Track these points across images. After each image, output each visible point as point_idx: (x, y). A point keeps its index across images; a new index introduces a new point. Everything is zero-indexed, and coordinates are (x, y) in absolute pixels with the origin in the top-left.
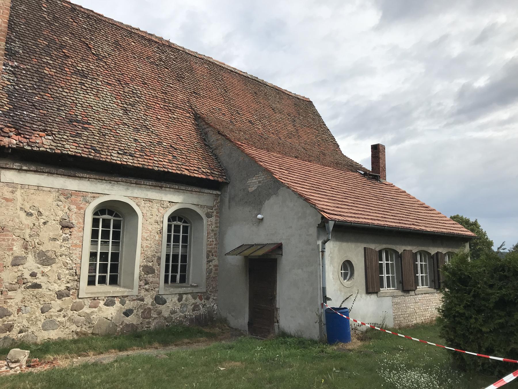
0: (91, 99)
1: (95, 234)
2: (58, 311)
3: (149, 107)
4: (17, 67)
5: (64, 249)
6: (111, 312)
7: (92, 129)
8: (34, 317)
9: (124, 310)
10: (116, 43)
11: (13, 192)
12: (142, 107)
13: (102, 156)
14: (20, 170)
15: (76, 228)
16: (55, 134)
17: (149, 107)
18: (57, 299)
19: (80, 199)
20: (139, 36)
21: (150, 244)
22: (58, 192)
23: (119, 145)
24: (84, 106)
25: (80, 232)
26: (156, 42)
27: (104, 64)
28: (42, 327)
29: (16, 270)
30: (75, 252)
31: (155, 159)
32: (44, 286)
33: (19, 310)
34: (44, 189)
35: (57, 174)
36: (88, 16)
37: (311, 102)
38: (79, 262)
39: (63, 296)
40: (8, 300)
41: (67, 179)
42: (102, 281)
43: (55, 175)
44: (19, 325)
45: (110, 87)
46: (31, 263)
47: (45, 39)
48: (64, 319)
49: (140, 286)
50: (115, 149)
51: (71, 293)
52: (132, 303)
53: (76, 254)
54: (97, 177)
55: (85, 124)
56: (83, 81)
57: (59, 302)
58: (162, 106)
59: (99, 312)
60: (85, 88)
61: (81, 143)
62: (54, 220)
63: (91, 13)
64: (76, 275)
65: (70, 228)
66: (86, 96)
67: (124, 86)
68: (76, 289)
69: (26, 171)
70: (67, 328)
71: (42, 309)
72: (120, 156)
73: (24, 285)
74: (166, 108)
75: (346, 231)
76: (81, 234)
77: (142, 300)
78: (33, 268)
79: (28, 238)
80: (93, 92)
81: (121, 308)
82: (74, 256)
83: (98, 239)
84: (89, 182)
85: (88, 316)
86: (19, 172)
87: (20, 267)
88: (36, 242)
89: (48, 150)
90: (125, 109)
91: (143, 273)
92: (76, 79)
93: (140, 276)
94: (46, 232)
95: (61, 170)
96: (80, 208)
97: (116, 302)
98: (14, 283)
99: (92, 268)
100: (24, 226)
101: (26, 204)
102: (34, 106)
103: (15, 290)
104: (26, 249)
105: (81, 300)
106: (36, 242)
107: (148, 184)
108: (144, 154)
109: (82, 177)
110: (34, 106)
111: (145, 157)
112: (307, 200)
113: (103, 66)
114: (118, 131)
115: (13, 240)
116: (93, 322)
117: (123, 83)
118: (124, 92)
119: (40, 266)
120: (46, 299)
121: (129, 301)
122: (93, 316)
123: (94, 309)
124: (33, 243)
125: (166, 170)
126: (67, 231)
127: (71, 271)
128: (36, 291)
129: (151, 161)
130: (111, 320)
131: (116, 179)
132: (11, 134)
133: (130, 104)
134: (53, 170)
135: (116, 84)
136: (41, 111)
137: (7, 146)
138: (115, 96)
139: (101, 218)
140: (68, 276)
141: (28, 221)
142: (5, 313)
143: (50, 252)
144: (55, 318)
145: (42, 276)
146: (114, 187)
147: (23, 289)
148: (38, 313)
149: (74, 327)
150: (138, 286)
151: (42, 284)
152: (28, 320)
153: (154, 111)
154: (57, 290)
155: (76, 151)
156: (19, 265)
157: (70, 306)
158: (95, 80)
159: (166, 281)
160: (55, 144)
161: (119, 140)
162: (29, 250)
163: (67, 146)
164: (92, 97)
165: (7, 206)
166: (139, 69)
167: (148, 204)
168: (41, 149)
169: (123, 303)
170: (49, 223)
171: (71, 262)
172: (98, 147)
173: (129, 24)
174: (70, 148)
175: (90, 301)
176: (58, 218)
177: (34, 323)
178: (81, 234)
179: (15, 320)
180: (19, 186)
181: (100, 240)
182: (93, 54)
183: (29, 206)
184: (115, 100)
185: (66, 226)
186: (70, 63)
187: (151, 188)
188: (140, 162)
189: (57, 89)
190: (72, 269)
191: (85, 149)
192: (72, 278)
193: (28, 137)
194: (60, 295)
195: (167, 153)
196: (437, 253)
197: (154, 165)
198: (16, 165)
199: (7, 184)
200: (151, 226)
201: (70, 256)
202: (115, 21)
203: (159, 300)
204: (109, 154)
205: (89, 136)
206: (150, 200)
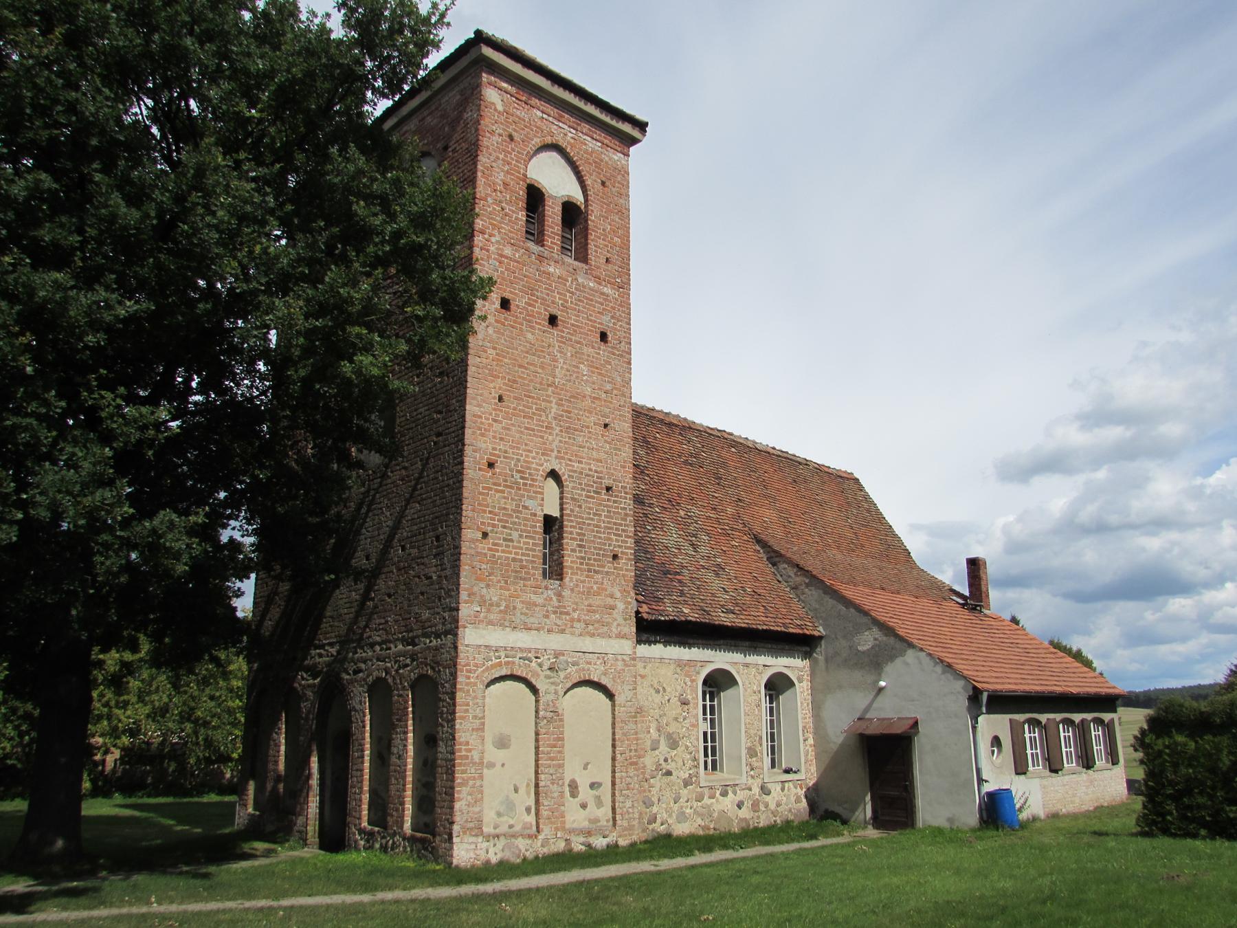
37: (857, 480)
75: (1001, 702)
77: (750, 789)
85: (709, 806)
112: (949, 666)
141: (658, 699)
149: (699, 821)
159: (706, 768)
194: (686, 783)
196: (1083, 721)
203: (765, 790)
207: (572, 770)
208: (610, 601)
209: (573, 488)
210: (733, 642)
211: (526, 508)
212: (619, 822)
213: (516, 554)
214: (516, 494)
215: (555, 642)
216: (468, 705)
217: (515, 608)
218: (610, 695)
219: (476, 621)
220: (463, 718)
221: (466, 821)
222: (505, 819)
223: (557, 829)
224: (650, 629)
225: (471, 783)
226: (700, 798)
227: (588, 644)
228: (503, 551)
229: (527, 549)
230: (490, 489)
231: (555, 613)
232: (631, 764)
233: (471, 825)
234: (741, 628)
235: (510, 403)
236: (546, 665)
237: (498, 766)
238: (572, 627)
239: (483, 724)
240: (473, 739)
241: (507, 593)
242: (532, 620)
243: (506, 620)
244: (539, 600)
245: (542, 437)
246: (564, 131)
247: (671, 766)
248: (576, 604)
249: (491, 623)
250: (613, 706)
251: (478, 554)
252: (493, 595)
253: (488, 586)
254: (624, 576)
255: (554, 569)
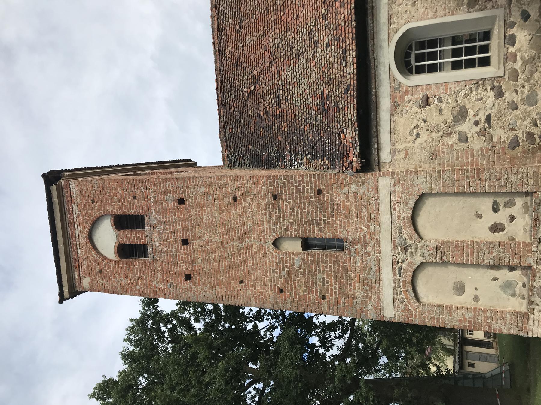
0: (297, 90)
1: (433, 69)
2: (517, 94)
3: (288, 30)
4: (290, 152)
5: (450, 100)
6: (523, 37)
7: (327, 91)
8: (521, 115)
9: (522, 21)
10: (236, 65)
11: (399, 152)
12: (291, 37)
13: (352, 83)
14: (378, 149)
15: (428, 92)
16: (340, 126)
17: (288, 30)
18: (504, 97)
19: (398, 93)
20: (220, 42)
21: (441, 6)
22: (393, 115)
23: (336, 64)
24: (306, 97)
25: (431, 87)
26: (218, 23)
27: (261, 78)
28: (533, 106)
29: (472, 139)
30: (452, 89)
31: (343, 25)
32: (489, 112)
33: (513, 129)
34: (392, 127)
35: (377, 119)
36: (223, 93)
38: (463, 83)
39: (501, 91)
40: (502, 141)
41: (380, 109)
42: (485, 49)
43: (378, 120)
44: (528, 128)
45: (281, 71)
46: (466, 127)
47: (259, 130)
48: (526, 87)
49: (493, 7)
50: (342, 69)
51: (498, 85)
52: (513, 13)
53: (455, 88)
54: (373, 81)
55: (324, 98)
56: (284, 98)
57: (507, 95)
58: (282, 13)
59: (521, 51)
60: (289, 96)
61: (343, 103)
62: (421, 114)
63: (219, 90)
64: (478, 83)
65: (428, 98)
66: (296, 95)
67: (274, 57)
68: (494, 80)
69: (378, 144)
70: (537, 82)
71: (513, 110)
72: (348, 64)
73: (487, 129)
74: (282, 8)
76: (434, 87)
78: (469, 125)
79: (441, 133)
80: (291, 88)
81: (519, 26)
82: (457, 89)
83: (437, 63)
84: (380, 88)
85: (525, 62)
86: (380, 149)
87: (469, 135)
88: (444, 126)
89: (357, 133)
90: (297, 55)
91: (477, 7)
92: (284, 105)
93: (481, 10)
94: (434, 119)
95: (373, 115)
96: (407, 92)
97: (511, 33)
98: (484, 138)
99: (471, 64)
100: (429, 139)
101: (408, 140)
102: (319, 140)
103: (492, 136)
104: (451, 133)
105: (507, 73)
106: (444, 126)
107: (372, 25)
108: (341, 38)
109: (376, 96)
110: (319, 140)
111: (343, 36)
113: (263, 79)
114: (323, 65)
115: (443, 145)
116: (533, 55)
117: (272, 59)
118: (281, 57)
119: (468, 119)
120: (503, 107)
121: (510, 17)
122: (526, 56)
123: (518, 57)
124: (445, 128)
125: (353, 11)
126: (431, 100)
127: (473, 89)
128: (493, 118)
129: (347, 29)
130: (533, 35)
131: (372, 62)
132: (349, 161)
133: (291, 50)
134: (374, 123)
135: (275, 65)
136: (322, 135)
137: (360, 165)
138: (288, 67)
139: (414, 64)
140: (479, 91)
141: (424, 136)
142: (516, 140)
143: (454, 112)
144: (524, 95)
145: (478, 115)
146: (381, 61)
147: (491, 130)
148: (517, 112)
150: (493, 10)
151: (487, 114)
152: (524, 120)
153: (290, 22)
154: (494, 99)
155: (352, 108)
156: (467, 137)
157: (512, 83)
158: (279, 86)
160: (350, 126)
161: (331, 64)
162: (452, 131)
163: (349, 116)
164: (296, 90)
165: (411, 154)
166: (252, 41)
167: (394, 19)
168: (357, 138)
169: (513, 25)
170: (425, 118)
171: (463, 91)
172: (343, 88)
173: (213, 54)
174: (351, 113)
175: (509, 62)
176: (419, 110)
177: (529, 114)
178: (434, 87)
179: (523, 131)
180: (393, 147)
181: (438, 61)
182: (255, 88)
183: (410, 137)
184: (292, 66)
185: (426, 102)
186: (271, 109)
187: (376, 20)
188: (351, 42)
189: (298, 121)
190: (471, 89)
191: (349, 100)
192: (481, 87)
193: (348, 149)
194: (499, 94)
195: (334, 8)
197: (350, 26)
198: (375, 152)
199: (392, 157)
200: (419, 10)
201: (456, 93)
202: (216, 67)
204: (349, 76)
205: (335, 94)
206: (390, 18)
207: (480, 232)
208: (351, 197)
209: (280, 228)
210: (370, 42)
211: (301, 266)
212: (529, 189)
213: (331, 276)
214: (294, 273)
215: (386, 247)
216: (434, 318)
217: (366, 279)
218: (422, 197)
219: (379, 308)
220: (443, 323)
221: (517, 326)
222: (517, 290)
223: (530, 251)
224: (368, 162)
225: (489, 320)
226: (515, 75)
227: (385, 219)
228: (331, 285)
229: (327, 267)
230: (295, 292)
231: (366, 247)
232: (479, 176)
233: (520, 322)
234: (357, 45)
235: (242, 277)
236: (402, 255)
237: (477, 293)
238: (374, 233)
239: (447, 307)
240: (459, 316)
241: (357, 284)
242: (373, 266)
243: (374, 285)
244: (358, 259)
245: (256, 252)
246: (81, 250)
247: (482, 116)
248: (357, 228)
249: (378, 297)
250: (431, 194)
251: (336, 304)
252: (360, 294)
253: (355, 298)
254: (331, 185)
255: (336, 245)
